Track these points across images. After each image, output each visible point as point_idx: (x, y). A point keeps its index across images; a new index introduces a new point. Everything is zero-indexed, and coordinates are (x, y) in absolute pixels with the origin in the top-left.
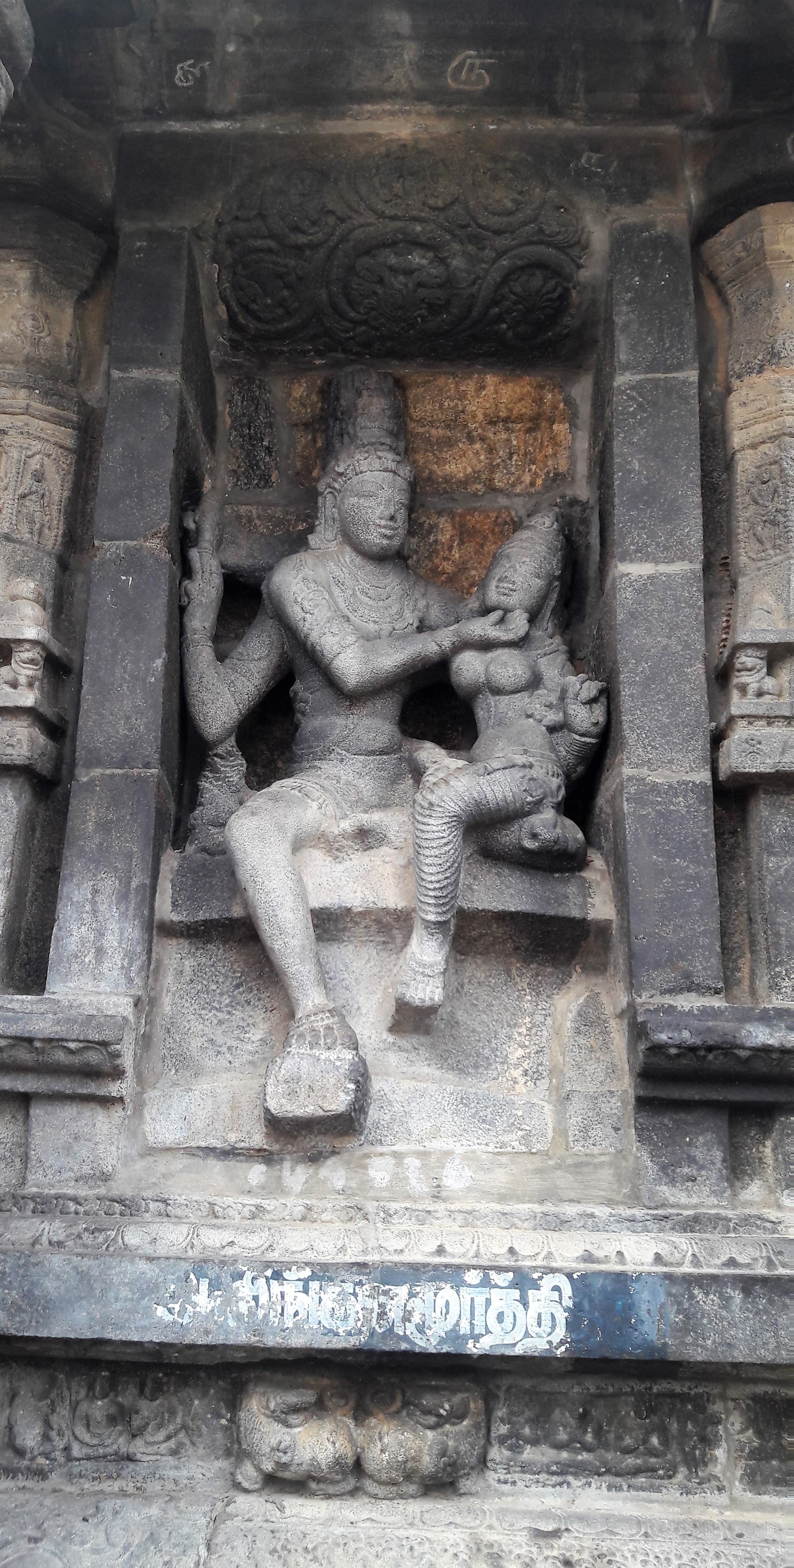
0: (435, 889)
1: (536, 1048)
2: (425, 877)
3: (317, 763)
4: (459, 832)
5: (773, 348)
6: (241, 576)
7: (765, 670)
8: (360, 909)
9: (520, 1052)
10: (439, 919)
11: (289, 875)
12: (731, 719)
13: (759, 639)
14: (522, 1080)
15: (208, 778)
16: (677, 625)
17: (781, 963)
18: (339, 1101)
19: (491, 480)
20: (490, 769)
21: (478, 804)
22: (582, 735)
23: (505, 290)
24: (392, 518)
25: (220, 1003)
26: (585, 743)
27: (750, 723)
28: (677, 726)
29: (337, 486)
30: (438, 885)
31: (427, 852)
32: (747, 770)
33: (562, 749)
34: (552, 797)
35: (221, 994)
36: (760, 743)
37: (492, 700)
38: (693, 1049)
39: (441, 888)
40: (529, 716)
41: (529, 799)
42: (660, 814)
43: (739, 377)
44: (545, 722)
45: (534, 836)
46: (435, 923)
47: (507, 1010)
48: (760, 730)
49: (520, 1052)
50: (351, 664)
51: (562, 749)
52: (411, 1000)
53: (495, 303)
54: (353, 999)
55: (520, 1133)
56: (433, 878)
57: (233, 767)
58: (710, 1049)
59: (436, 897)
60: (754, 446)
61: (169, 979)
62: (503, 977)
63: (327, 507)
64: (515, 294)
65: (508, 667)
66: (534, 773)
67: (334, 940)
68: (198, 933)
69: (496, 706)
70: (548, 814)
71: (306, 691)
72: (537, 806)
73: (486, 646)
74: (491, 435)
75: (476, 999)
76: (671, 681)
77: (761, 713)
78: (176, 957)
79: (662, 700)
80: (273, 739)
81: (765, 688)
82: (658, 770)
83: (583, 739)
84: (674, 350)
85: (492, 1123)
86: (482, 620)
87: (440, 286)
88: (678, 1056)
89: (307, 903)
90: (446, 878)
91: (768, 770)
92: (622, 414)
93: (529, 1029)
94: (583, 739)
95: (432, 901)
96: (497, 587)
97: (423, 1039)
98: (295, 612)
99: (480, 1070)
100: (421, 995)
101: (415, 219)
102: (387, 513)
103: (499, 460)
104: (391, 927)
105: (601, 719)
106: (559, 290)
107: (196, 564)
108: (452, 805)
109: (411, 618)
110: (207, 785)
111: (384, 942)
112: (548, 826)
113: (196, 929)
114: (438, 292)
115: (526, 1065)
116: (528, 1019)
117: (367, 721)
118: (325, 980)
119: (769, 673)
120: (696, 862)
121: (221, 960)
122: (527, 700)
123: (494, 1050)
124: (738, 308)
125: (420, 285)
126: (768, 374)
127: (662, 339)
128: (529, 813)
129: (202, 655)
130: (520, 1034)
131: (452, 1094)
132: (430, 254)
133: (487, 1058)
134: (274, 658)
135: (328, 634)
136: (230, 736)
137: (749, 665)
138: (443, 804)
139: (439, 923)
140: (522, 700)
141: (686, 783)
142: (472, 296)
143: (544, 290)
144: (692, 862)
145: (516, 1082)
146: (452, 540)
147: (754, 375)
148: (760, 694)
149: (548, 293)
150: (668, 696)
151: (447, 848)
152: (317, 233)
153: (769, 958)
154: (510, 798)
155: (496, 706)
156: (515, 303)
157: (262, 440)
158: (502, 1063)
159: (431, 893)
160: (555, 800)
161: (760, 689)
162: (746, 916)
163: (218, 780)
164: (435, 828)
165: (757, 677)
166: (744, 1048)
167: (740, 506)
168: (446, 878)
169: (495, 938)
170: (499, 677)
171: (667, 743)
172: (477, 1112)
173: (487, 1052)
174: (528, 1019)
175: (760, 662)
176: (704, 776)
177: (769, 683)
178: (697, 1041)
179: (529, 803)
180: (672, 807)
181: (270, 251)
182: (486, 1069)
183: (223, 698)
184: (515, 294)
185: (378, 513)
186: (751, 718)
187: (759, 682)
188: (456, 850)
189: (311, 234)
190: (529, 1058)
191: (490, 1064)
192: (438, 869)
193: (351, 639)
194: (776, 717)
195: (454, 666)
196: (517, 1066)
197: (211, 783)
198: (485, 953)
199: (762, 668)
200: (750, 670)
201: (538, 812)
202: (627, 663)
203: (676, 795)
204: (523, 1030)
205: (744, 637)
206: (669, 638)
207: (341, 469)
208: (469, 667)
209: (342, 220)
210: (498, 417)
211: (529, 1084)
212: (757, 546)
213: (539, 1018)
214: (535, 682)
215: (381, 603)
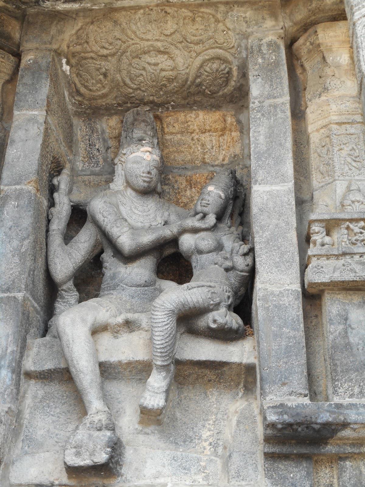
0: (160, 348)
1: (217, 431)
2: (155, 342)
3: (112, 292)
4: (174, 319)
5: (325, 86)
6: (81, 206)
7: (325, 233)
8: (126, 361)
9: (208, 433)
10: (165, 363)
11: (87, 344)
12: (309, 257)
13: (320, 217)
14: (208, 448)
15: (59, 302)
16: (282, 213)
17: (338, 380)
18: (102, 457)
19: (204, 158)
20: (190, 287)
21: (183, 305)
22: (241, 271)
23: (202, 70)
24: (149, 173)
25: (54, 412)
26: (243, 276)
27: (318, 259)
28: (283, 262)
29: (123, 160)
30: (162, 346)
31: (156, 329)
32: (316, 281)
33: (232, 279)
34: (225, 302)
35: (56, 408)
36: (322, 267)
37: (199, 257)
38: (290, 425)
39: (163, 348)
40: (216, 264)
41: (212, 302)
42: (276, 306)
43: (310, 101)
44: (224, 266)
45: (215, 321)
46: (161, 366)
47: (204, 412)
48: (323, 262)
49: (208, 433)
50: (126, 241)
51: (232, 279)
52: (147, 405)
53: (197, 77)
54: (122, 408)
55: (203, 474)
56: (159, 343)
57: (72, 296)
58: (299, 424)
59: (161, 352)
60: (318, 130)
61: (28, 401)
62: (203, 395)
63: (119, 170)
64: (206, 72)
65: (205, 241)
66: (215, 290)
67: (115, 379)
68: (44, 376)
69: (200, 260)
70: (223, 310)
71: (108, 257)
72: (217, 306)
73: (195, 231)
74: (203, 138)
75: (188, 407)
76: (280, 240)
77: (323, 253)
78: (34, 390)
79: (276, 250)
80: (89, 279)
81: (325, 242)
82: (277, 285)
83: (242, 274)
84: (278, 89)
85: (189, 470)
86: (194, 218)
87: (172, 70)
88: (282, 428)
89: (97, 357)
90: (166, 342)
91: (327, 281)
92: (254, 119)
93: (214, 422)
94: (242, 274)
95: (159, 355)
96: (201, 203)
97: (157, 428)
98: (100, 218)
99: (187, 443)
100: (152, 403)
101: (157, 40)
102: (146, 171)
103: (207, 150)
104: (141, 370)
105: (250, 263)
106: (227, 70)
107: (57, 200)
108: (169, 305)
109: (160, 220)
110: (59, 305)
111: (140, 379)
112: (224, 317)
113: (44, 375)
114: (171, 73)
115: (211, 440)
116: (214, 417)
117: (136, 270)
118: (105, 397)
119: (328, 234)
120: (294, 329)
121: (55, 388)
122: (215, 256)
123: (194, 433)
124: (310, 71)
125: (162, 70)
126: (323, 98)
127: (271, 85)
128: (212, 310)
129: (56, 240)
130: (209, 424)
131: (169, 455)
132: (166, 56)
133: (190, 437)
134: (92, 241)
135: (115, 227)
136: (69, 280)
137: (317, 231)
138: (165, 305)
139: (164, 366)
140: (213, 256)
141: (288, 290)
142: (188, 74)
143: (220, 70)
144: (292, 330)
145: (205, 449)
146: (186, 187)
147: (317, 99)
148: (323, 245)
149: (222, 70)
150: (279, 248)
151: (167, 327)
152: (112, 49)
153: (332, 378)
154: (201, 301)
155: (200, 260)
156: (207, 76)
157: (95, 146)
158: (198, 439)
159: (159, 351)
160: (227, 304)
161: (322, 242)
162: (323, 358)
163: (64, 302)
164: (160, 317)
165: (321, 236)
166: (316, 424)
167: (313, 159)
168: (166, 342)
169: (198, 375)
170: (200, 245)
171: (279, 270)
172: (181, 464)
173: (191, 434)
174: (214, 417)
175: (322, 229)
176: (297, 287)
177: (327, 239)
178: (291, 420)
179: (212, 305)
180: (281, 302)
181: (92, 58)
182: (190, 442)
183: (65, 262)
184: (206, 72)
185: (142, 170)
186: (319, 256)
187: (322, 238)
188: (172, 328)
189: (110, 49)
190: (213, 436)
191: (192, 440)
192: (161, 338)
193: (126, 229)
194: (331, 255)
195: (180, 242)
196: (206, 441)
197: (60, 304)
198: (193, 384)
199: (323, 232)
200: (317, 233)
201: (218, 310)
202: (258, 232)
203: (283, 296)
204: (211, 422)
205: (313, 217)
206: (279, 220)
207: (124, 152)
208: (187, 242)
209: (124, 42)
210: (206, 130)
211: (212, 449)
212: (321, 176)
213: (219, 416)
214: (219, 247)
215: (145, 214)
